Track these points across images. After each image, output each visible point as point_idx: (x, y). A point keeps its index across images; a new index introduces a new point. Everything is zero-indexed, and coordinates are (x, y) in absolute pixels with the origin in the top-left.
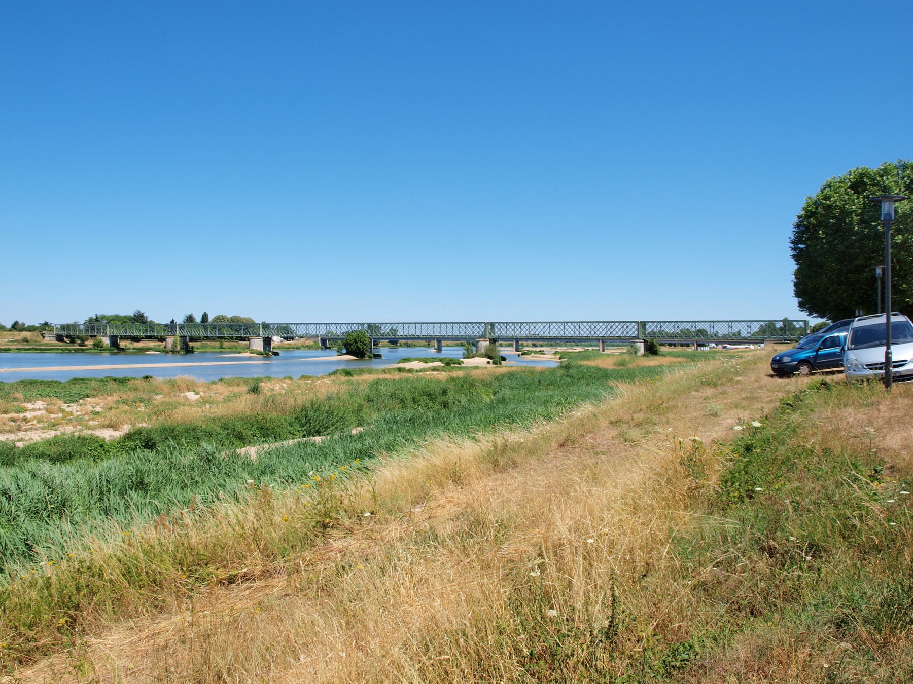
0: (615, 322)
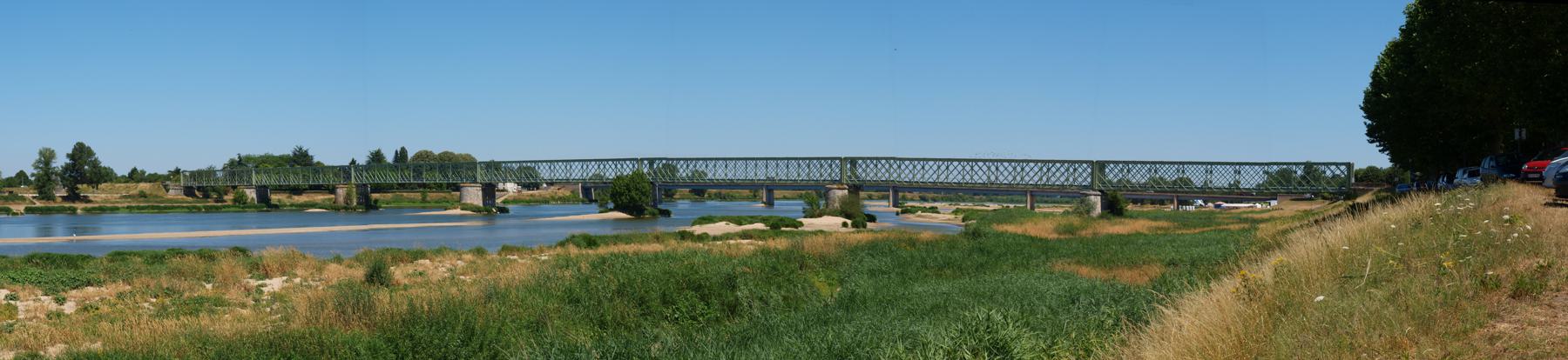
0: (1054, 162)
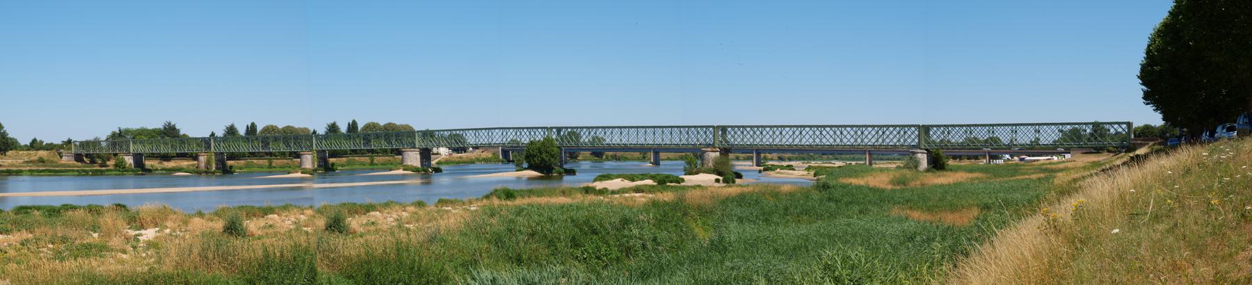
0: (888, 126)
